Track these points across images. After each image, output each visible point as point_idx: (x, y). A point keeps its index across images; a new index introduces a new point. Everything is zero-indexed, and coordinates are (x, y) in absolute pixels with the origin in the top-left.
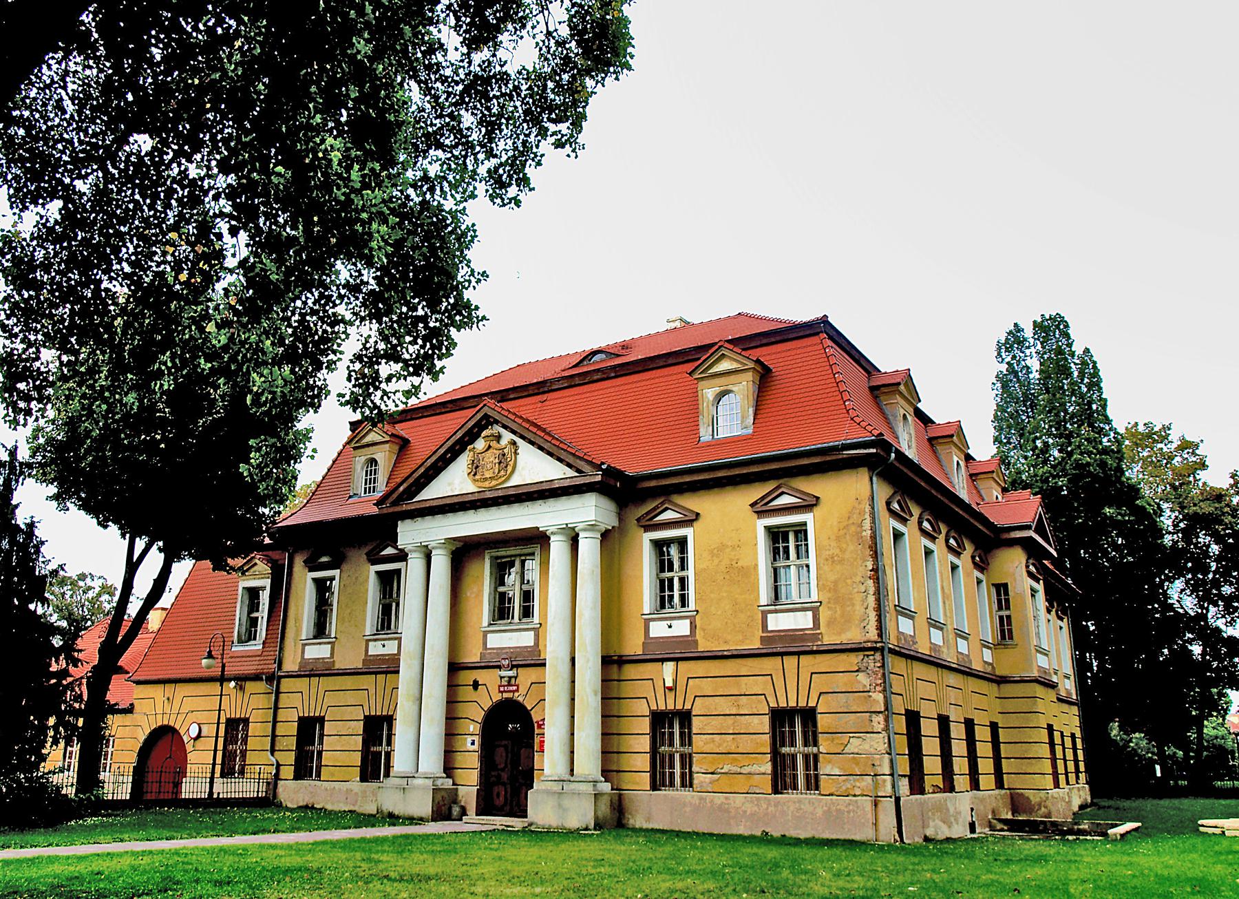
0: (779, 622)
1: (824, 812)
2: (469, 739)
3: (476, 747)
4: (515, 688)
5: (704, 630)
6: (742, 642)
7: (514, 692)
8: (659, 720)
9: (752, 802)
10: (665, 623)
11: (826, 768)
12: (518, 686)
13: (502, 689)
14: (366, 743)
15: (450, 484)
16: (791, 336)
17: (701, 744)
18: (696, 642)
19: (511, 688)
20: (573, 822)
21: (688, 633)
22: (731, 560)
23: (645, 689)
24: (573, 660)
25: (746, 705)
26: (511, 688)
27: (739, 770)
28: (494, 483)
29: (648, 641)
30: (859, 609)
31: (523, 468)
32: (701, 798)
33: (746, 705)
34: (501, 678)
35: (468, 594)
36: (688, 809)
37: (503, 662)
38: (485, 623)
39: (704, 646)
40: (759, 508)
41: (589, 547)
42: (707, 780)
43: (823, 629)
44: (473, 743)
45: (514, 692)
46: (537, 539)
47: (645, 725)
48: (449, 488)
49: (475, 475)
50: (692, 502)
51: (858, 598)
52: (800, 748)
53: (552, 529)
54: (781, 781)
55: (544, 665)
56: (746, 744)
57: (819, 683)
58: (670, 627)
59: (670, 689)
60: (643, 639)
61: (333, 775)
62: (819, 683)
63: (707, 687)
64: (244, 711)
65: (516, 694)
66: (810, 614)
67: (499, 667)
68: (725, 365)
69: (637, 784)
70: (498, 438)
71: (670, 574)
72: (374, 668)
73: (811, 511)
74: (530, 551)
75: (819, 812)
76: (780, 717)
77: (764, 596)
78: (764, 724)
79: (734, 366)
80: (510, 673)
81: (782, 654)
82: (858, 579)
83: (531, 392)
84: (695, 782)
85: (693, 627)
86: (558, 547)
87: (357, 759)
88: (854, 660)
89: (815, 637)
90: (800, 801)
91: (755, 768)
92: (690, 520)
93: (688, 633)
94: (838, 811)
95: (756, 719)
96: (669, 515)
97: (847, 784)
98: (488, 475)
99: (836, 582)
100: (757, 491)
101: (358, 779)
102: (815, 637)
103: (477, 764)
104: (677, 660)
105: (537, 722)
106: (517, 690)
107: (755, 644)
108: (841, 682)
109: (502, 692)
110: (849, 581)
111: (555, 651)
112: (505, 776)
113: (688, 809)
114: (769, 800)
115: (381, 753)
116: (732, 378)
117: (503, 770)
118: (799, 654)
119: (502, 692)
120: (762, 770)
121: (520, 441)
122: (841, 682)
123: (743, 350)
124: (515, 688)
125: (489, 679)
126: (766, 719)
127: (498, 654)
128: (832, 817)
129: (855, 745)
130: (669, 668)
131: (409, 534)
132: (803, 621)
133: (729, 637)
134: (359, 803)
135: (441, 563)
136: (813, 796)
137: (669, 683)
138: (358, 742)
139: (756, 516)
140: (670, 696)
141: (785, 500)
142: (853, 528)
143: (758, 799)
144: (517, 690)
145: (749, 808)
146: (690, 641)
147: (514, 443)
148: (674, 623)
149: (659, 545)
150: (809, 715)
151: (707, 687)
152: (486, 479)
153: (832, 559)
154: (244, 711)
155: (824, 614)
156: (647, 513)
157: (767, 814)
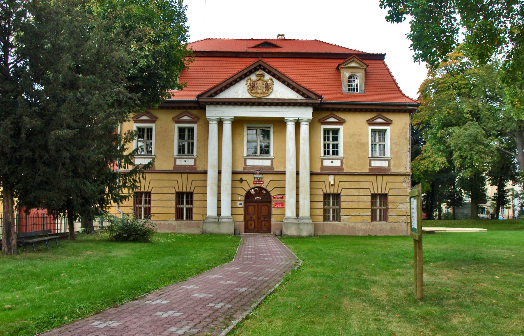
0: (375, 164)
1: (390, 228)
2: (239, 203)
3: (243, 205)
4: (262, 182)
5: (346, 164)
6: (362, 170)
7: (261, 184)
8: (326, 196)
9: (364, 225)
10: (330, 161)
11: (390, 213)
12: (263, 182)
13: (255, 183)
14: (372, 205)
15: (236, 93)
16: (241, 56)
17: (344, 205)
18: (343, 169)
19: (260, 182)
20: (304, 233)
21: (340, 165)
22: (358, 140)
23: (322, 185)
24: (298, 174)
25: (362, 192)
26: (260, 182)
27: (359, 214)
28: (262, 95)
29: (323, 167)
30: (404, 161)
31: (276, 91)
32: (344, 224)
33: (362, 192)
34: (254, 178)
35: (235, 142)
36: (339, 228)
37: (257, 171)
38: (245, 155)
39: (346, 170)
40: (370, 122)
41: (304, 128)
42: (346, 218)
43: (391, 168)
44: (241, 204)
45: (261, 184)
46: (281, 123)
47: (321, 198)
48: (235, 94)
49: (252, 90)
50: (343, 116)
51: (404, 158)
52: (143, 205)
53: (213, 118)
54: (179, 215)
55: (285, 174)
56: (362, 205)
57: (389, 186)
58: (332, 162)
59: (332, 185)
60: (243, 166)
61: (158, 217)
62: (389, 186)
63: (347, 185)
64: (189, 187)
65: (263, 185)
66: (193, 160)
67: (254, 174)
68: (353, 65)
69: (318, 220)
70: (263, 76)
71: (328, 142)
72: (180, 170)
73: (342, 125)
74: (269, 126)
75: (388, 228)
76: (374, 196)
77: (370, 155)
78: (369, 199)
79: (357, 65)
80: (260, 176)
81: (376, 175)
82: (405, 151)
83: (252, 56)
84: (342, 219)
85: (342, 163)
86: (290, 128)
87: (173, 211)
88: (402, 178)
89: (389, 170)
90: (381, 224)
91: (365, 214)
92: (341, 122)
93: (340, 165)
94: (395, 227)
95: (366, 197)
96: (332, 120)
97: (397, 219)
98: (259, 91)
99: (397, 152)
100: (369, 116)
101: (174, 219)
102: (389, 170)
103: (243, 213)
104: (335, 175)
105: (273, 196)
106: (263, 183)
107: (366, 171)
108: (397, 185)
109: (255, 184)
110: (401, 152)
111: (290, 168)
112: (254, 217)
113: (339, 228)
114: (371, 224)
115: (183, 208)
116: (356, 70)
117: (253, 215)
118: (383, 175)
119: (255, 184)
120: (368, 214)
121: (274, 80)
122: (397, 185)
123: (362, 59)
124: (262, 182)
125: (249, 179)
126: (370, 197)
127: (253, 168)
128: (392, 229)
129: (401, 206)
130: (331, 179)
131: (212, 113)
132: (385, 164)
133: (356, 168)
134: (176, 229)
135: (227, 127)
136: (383, 223)
137: (332, 183)
138: (173, 203)
139: (368, 125)
140: (332, 188)
141: (379, 120)
142: (403, 134)
143: (366, 224)
144: (263, 183)
145: (364, 227)
146: (340, 168)
147: (272, 80)
148: (334, 161)
149: (326, 131)
150: (385, 196)
151: (347, 185)
152: (258, 93)
153: (395, 144)
154: (189, 187)
155: (392, 162)
156: (324, 118)
157: (370, 229)
